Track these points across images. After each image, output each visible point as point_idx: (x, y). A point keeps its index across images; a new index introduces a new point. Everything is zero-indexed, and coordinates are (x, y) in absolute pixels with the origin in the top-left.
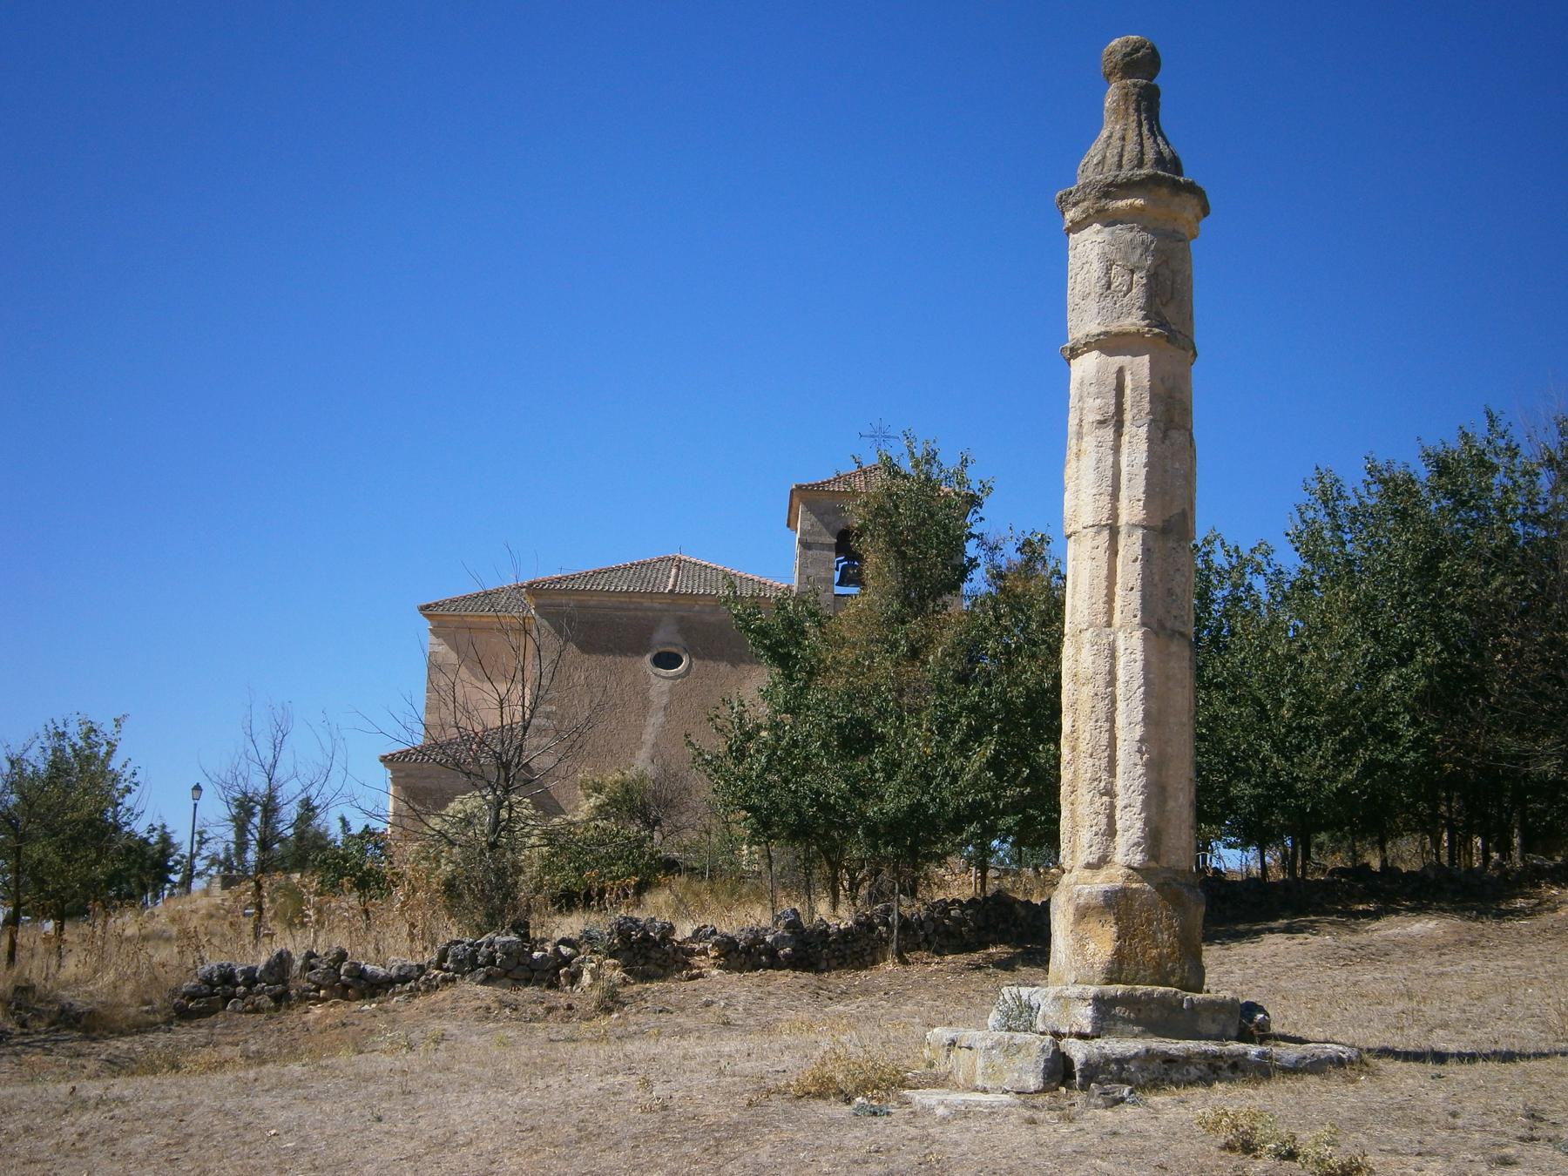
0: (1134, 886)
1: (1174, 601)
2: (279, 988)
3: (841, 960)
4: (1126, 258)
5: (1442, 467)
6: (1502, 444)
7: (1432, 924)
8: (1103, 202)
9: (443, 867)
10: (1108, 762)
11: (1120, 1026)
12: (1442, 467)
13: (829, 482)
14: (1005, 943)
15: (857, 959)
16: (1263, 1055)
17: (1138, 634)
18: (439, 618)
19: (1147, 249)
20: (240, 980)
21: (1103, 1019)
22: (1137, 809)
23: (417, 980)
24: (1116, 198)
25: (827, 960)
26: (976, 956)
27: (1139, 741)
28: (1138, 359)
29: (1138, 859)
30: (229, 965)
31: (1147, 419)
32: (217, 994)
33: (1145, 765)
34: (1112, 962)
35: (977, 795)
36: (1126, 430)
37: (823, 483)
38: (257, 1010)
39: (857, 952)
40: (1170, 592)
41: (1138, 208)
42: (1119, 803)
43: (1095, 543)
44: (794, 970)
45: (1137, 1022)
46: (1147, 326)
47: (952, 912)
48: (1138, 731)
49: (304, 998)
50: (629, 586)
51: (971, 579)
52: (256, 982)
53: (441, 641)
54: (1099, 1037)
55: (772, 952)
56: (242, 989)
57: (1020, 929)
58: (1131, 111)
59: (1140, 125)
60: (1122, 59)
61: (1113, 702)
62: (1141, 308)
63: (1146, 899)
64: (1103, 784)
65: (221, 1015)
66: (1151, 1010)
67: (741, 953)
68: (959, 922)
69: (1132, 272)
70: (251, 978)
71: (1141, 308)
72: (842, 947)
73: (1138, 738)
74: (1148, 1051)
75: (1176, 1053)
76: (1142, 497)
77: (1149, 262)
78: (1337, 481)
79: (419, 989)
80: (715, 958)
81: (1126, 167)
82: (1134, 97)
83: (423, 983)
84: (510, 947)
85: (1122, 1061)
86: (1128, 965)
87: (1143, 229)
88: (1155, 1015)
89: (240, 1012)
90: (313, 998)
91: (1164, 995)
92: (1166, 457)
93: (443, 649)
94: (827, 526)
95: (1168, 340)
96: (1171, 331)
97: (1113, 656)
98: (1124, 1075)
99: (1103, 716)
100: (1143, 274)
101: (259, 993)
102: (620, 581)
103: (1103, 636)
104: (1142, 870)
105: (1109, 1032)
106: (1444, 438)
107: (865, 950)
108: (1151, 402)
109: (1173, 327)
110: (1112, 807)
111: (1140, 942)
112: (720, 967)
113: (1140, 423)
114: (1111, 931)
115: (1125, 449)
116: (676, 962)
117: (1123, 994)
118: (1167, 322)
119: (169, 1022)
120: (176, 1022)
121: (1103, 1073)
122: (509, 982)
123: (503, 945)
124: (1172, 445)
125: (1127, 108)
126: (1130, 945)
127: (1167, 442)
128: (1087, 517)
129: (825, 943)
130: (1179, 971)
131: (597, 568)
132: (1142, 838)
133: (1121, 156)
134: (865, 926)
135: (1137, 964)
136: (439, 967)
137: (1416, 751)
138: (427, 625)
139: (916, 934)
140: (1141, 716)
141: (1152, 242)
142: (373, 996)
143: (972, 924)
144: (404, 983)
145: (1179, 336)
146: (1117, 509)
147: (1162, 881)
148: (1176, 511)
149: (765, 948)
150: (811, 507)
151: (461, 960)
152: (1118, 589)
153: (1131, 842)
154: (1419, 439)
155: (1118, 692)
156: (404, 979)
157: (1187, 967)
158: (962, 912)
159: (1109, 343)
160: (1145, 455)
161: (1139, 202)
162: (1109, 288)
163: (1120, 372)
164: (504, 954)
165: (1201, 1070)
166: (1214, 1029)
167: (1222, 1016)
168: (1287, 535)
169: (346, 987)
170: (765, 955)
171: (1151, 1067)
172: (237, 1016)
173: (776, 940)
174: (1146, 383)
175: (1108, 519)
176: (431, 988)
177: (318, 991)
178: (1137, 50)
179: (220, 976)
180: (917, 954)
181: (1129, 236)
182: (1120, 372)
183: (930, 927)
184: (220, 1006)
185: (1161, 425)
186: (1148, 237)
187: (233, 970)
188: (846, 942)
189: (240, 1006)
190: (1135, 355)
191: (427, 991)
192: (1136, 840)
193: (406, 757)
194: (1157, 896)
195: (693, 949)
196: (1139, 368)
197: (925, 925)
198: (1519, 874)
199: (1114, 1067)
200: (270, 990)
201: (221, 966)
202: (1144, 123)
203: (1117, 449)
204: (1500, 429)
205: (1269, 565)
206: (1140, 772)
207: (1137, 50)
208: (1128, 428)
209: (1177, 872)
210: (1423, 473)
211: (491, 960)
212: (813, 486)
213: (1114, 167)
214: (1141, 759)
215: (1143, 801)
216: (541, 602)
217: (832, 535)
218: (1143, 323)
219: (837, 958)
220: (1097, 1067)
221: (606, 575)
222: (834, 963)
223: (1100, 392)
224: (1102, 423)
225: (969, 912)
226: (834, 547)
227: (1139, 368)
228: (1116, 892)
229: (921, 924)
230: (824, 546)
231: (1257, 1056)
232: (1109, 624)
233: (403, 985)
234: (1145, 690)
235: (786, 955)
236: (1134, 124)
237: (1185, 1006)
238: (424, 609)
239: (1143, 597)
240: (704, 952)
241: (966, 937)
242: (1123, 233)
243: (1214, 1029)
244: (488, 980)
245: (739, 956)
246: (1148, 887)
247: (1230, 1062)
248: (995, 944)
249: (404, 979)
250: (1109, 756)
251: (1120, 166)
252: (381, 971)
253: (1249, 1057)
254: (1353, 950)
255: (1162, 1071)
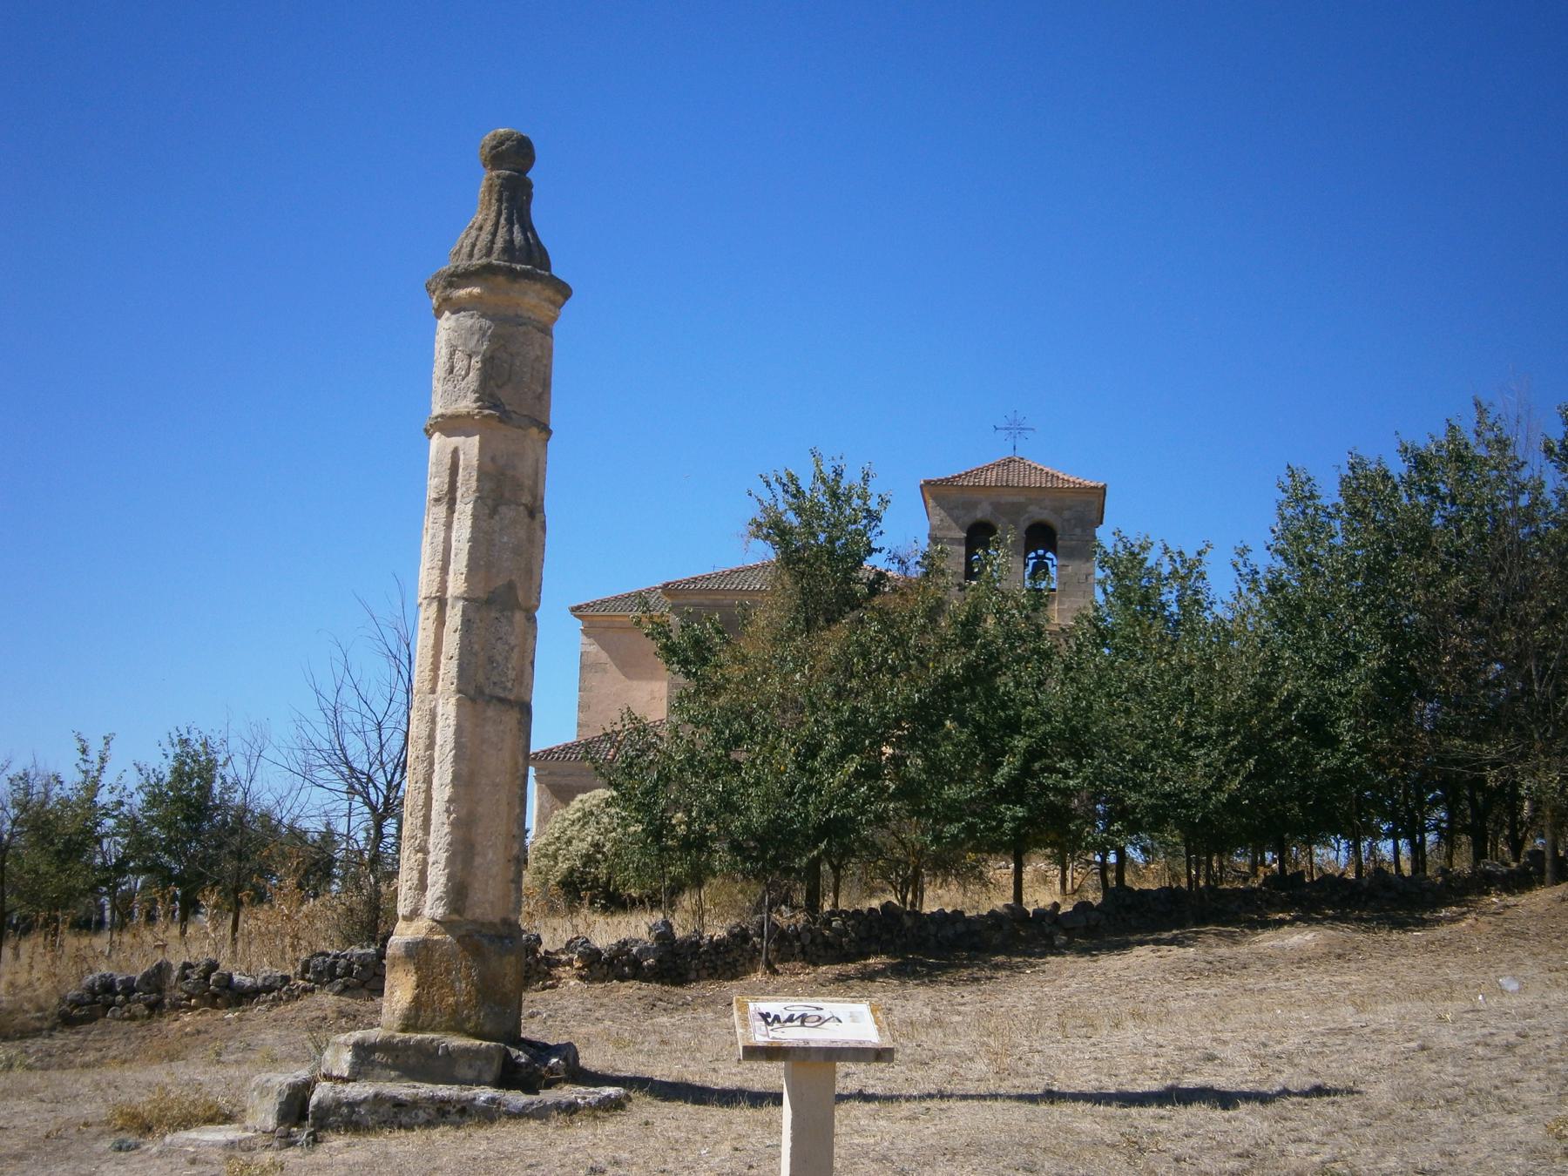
0: (436, 937)
1: (495, 668)
2: (154, 997)
3: (711, 971)
4: (465, 344)
5: (1421, 463)
6: (1490, 436)
7: (1309, 937)
8: (448, 291)
9: (560, 865)
10: (423, 821)
11: (378, 1071)
12: (1421, 463)
13: (960, 476)
14: (887, 953)
15: (729, 969)
16: (493, 1100)
17: (453, 700)
18: (589, 619)
19: (484, 335)
20: (119, 989)
21: (362, 1064)
22: (441, 866)
23: (280, 990)
24: (459, 287)
25: (697, 971)
26: (851, 968)
27: (448, 801)
28: (470, 440)
29: (440, 912)
30: (111, 975)
31: (472, 498)
32: (99, 1002)
33: (452, 824)
34: (409, 1009)
35: (838, 811)
36: (457, 507)
37: (954, 477)
38: (133, 1018)
39: (729, 963)
40: (491, 660)
41: (476, 297)
42: (431, 859)
43: (427, 614)
44: (663, 984)
45: (394, 1067)
46: (479, 408)
47: (834, 923)
48: (448, 792)
49: (176, 1007)
50: (762, 585)
51: (455, 631)
52: (134, 991)
53: (592, 640)
54: (355, 1081)
55: (636, 963)
56: (120, 998)
57: (904, 940)
58: (493, 201)
59: (499, 214)
60: (490, 152)
61: (431, 764)
62: (475, 392)
63: (446, 950)
64: (418, 841)
65: (100, 1022)
66: (408, 1057)
67: (604, 964)
68: (839, 933)
69: (470, 357)
70: (129, 988)
71: (475, 392)
72: (713, 958)
73: (446, 799)
74: (376, 1095)
75: (404, 1097)
76: (464, 570)
77: (485, 347)
78: (1309, 479)
79: (281, 999)
80: (579, 968)
81: (476, 256)
82: (497, 188)
83: (285, 993)
84: (365, 959)
85: (353, 1105)
86: (425, 1011)
87: (483, 316)
88: (412, 1061)
89: (118, 1019)
90: (185, 1006)
91: (420, 1042)
92: (494, 532)
93: (594, 648)
94: (956, 520)
95: (501, 420)
96: (505, 412)
97: (433, 721)
98: (354, 1117)
99: (421, 778)
100: (478, 358)
101: (135, 1002)
102: (754, 579)
103: (427, 702)
104: (445, 922)
105: (366, 1076)
106: (1427, 435)
107: (738, 960)
108: (478, 480)
109: (507, 408)
110: (425, 863)
111: (438, 990)
112: (581, 978)
113: (467, 500)
114: (412, 979)
115: (455, 526)
116: (539, 973)
117: (381, 1041)
118: (502, 404)
119: (53, 1028)
120: (59, 1028)
121: (334, 1114)
122: (366, 993)
123: (359, 957)
124: (501, 519)
125: (490, 199)
126: (428, 993)
127: (497, 517)
128: (423, 592)
129: (695, 955)
130: (474, 1018)
131: (734, 568)
132: (444, 892)
133: (474, 245)
134: (740, 937)
135: (434, 1010)
136: (303, 978)
137: (1360, 756)
138: (579, 624)
139: (791, 945)
140: (450, 778)
141: (489, 328)
142: (239, 1004)
143: (853, 935)
144: (268, 993)
145: (514, 416)
146: (446, 582)
147: (464, 933)
148: (500, 582)
149: (628, 960)
150: (941, 501)
151: (320, 972)
152: (443, 659)
153: (435, 896)
154: (1397, 433)
155: (436, 755)
156: (268, 989)
157: (482, 1014)
158: (844, 923)
159: (450, 425)
160: (469, 530)
161: (476, 290)
162: (451, 372)
163: (455, 452)
164: (361, 965)
165: (429, 1114)
166: (470, 1074)
167: (479, 1063)
168: (1273, 531)
169: (215, 996)
170: (628, 966)
171: (381, 1110)
172: (114, 1023)
173: (640, 951)
174: (475, 463)
175: (438, 591)
176: (292, 997)
177: (189, 999)
178: (502, 143)
179: (101, 986)
180: (790, 965)
181: (470, 322)
182: (455, 452)
183: (807, 938)
184: (100, 1013)
185: (490, 502)
186: (485, 323)
187: (113, 980)
188: (718, 953)
189: (118, 1013)
190: (468, 436)
191: (288, 1001)
192: (439, 895)
193: (549, 755)
194: (458, 948)
195: (559, 961)
196: (470, 447)
197: (802, 936)
198: (1466, 880)
199: (345, 1110)
200: (145, 999)
201: (104, 976)
202: (504, 212)
203: (448, 526)
204: (1490, 421)
205: (1245, 565)
206: (447, 830)
207: (502, 143)
208: (459, 506)
209: (483, 924)
210: (1398, 468)
211: (348, 971)
212: (942, 481)
213: (465, 257)
214: (448, 818)
215: (447, 858)
216: (676, 602)
217: (961, 528)
218: (475, 405)
219: (708, 968)
220: (328, 1110)
221: (742, 574)
222: (704, 973)
223: (437, 472)
224: (437, 500)
225: (852, 922)
226: (963, 541)
227: (470, 447)
228: (418, 943)
229: (798, 936)
230: (953, 541)
231: (484, 1102)
232: (433, 691)
233: (268, 994)
234: (455, 754)
235: (649, 965)
236: (494, 214)
237: (440, 1052)
238: (576, 610)
239: (461, 667)
240: (570, 963)
241: (846, 947)
242: (467, 320)
243: (470, 1074)
244: (345, 990)
245: (601, 967)
246: (449, 938)
247: (458, 1106)
248: (876, 954)
249: (268, 989)
250: (424, 815)
251: (471, 255)
252: (248, 981)
253: (476, 1102)
254: (1211, 963)
255: (391, 1115)
